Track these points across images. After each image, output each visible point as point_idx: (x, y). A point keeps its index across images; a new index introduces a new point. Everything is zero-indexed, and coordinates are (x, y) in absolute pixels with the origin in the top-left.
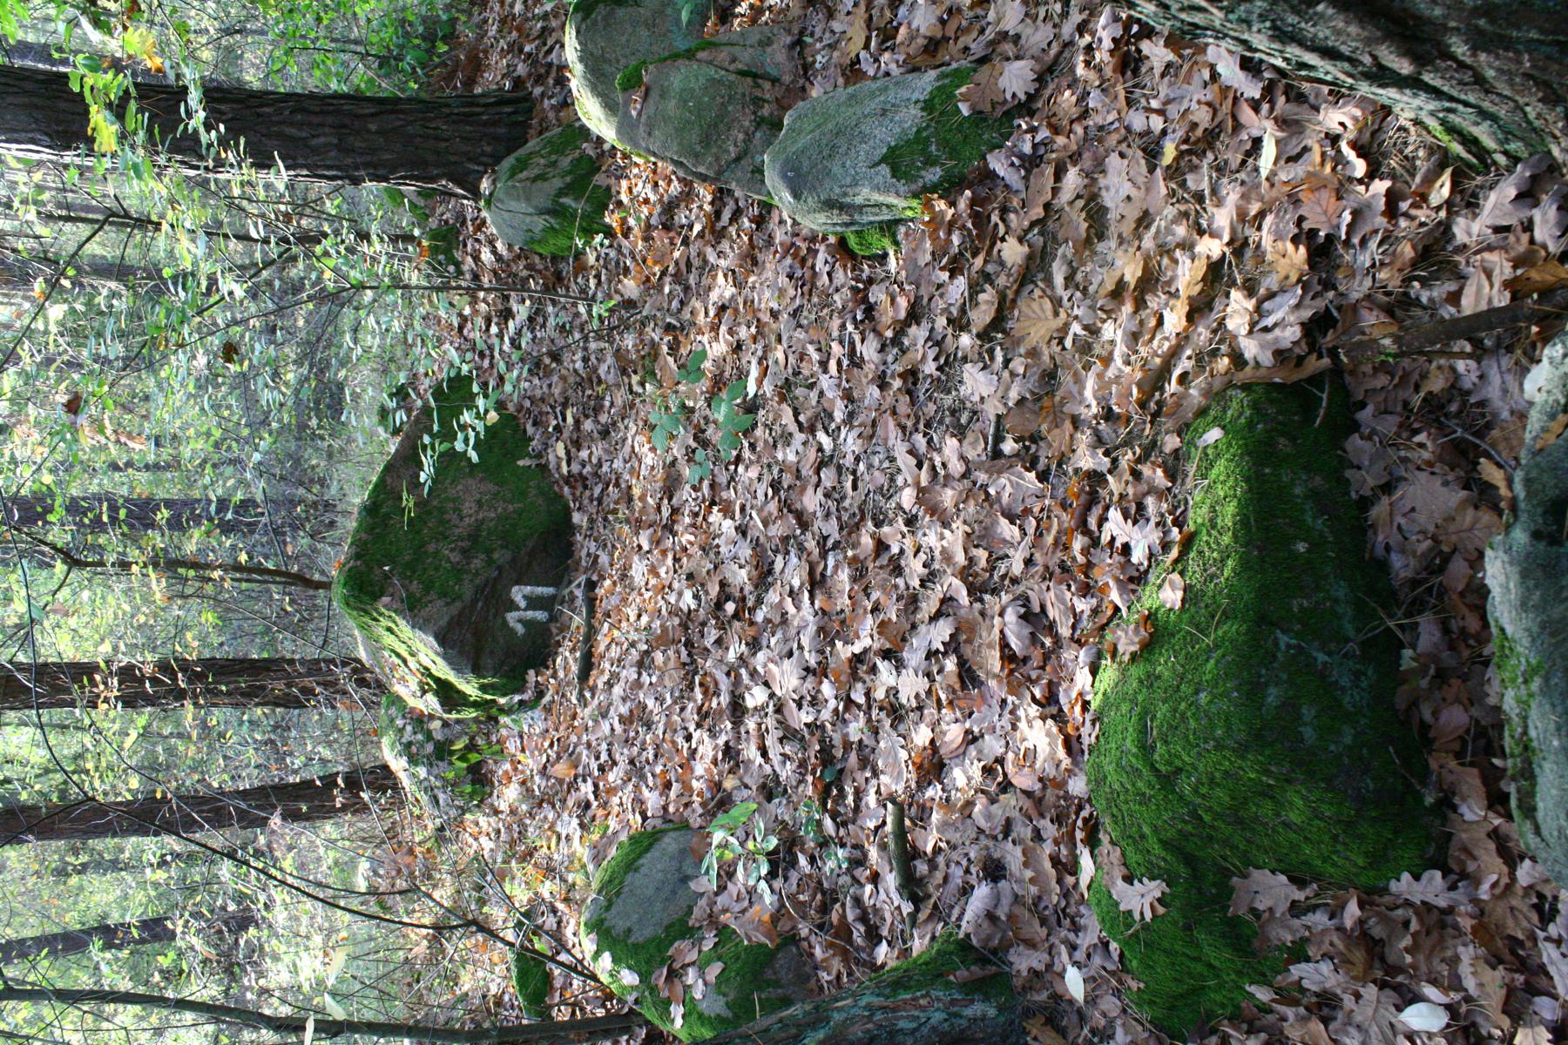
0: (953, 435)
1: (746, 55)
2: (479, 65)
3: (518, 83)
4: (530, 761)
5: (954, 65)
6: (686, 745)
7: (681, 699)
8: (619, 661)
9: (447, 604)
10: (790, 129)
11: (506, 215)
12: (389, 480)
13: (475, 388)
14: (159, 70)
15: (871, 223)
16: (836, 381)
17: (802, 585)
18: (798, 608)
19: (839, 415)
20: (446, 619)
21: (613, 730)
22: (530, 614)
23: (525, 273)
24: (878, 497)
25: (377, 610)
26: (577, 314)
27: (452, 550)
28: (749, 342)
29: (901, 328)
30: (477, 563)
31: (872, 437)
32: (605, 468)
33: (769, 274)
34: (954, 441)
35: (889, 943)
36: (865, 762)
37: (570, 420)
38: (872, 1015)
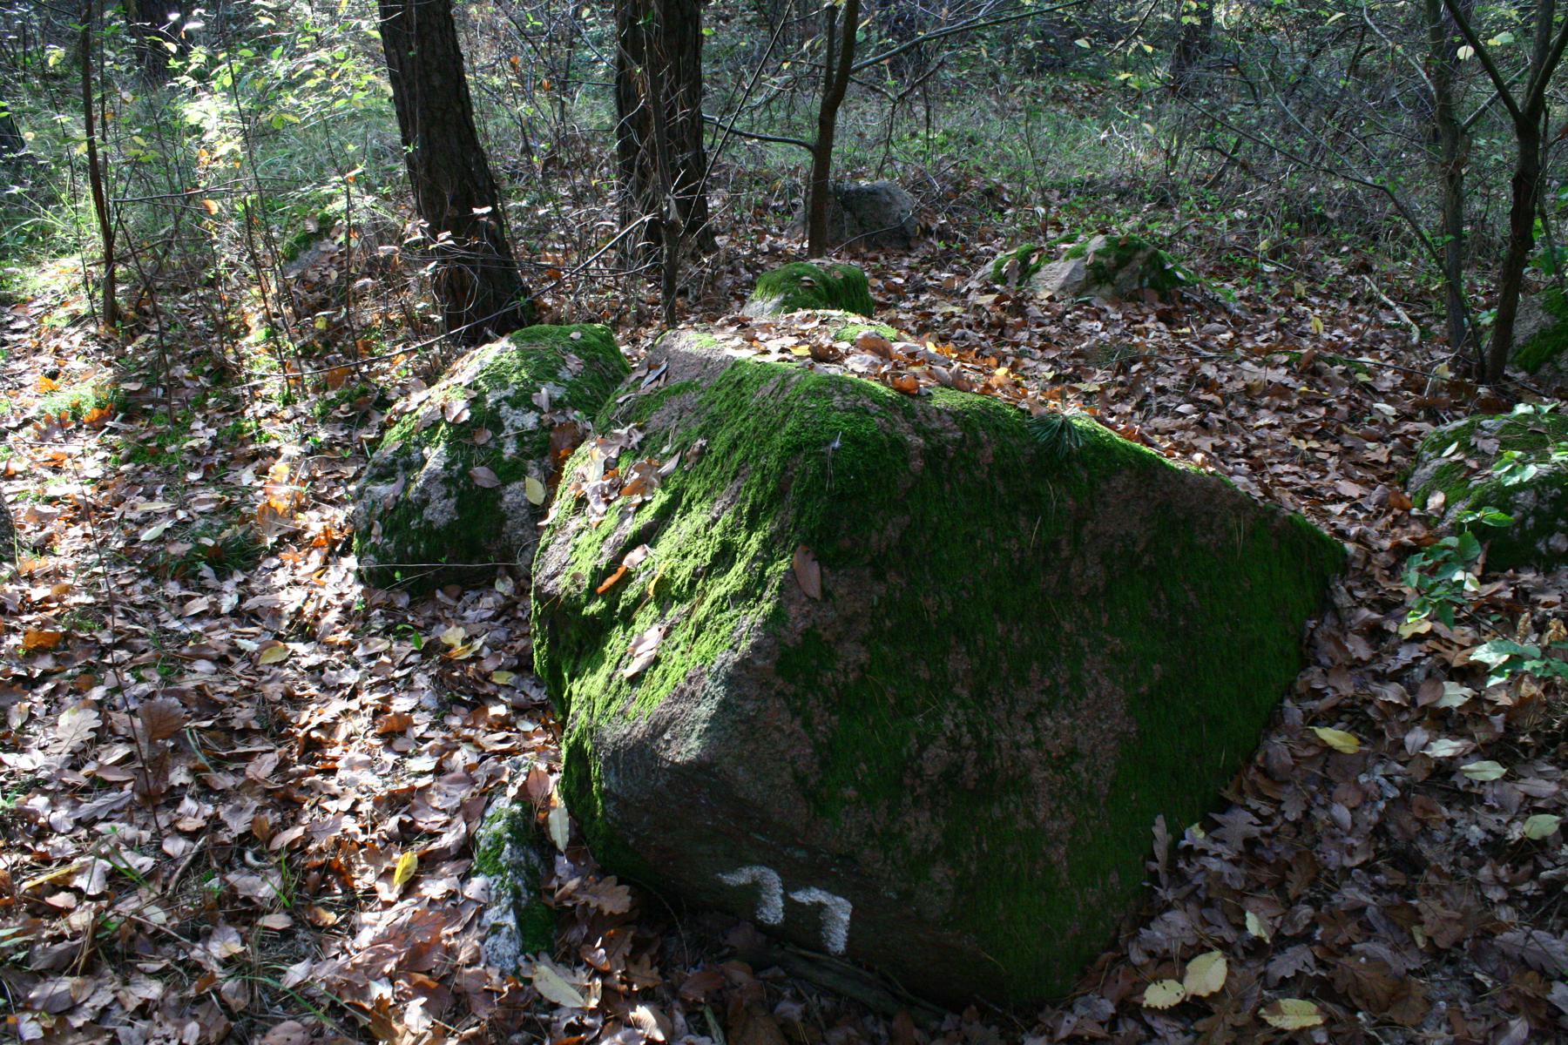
9: (799, 779)
27: (954, 743)
30: (922, 827)
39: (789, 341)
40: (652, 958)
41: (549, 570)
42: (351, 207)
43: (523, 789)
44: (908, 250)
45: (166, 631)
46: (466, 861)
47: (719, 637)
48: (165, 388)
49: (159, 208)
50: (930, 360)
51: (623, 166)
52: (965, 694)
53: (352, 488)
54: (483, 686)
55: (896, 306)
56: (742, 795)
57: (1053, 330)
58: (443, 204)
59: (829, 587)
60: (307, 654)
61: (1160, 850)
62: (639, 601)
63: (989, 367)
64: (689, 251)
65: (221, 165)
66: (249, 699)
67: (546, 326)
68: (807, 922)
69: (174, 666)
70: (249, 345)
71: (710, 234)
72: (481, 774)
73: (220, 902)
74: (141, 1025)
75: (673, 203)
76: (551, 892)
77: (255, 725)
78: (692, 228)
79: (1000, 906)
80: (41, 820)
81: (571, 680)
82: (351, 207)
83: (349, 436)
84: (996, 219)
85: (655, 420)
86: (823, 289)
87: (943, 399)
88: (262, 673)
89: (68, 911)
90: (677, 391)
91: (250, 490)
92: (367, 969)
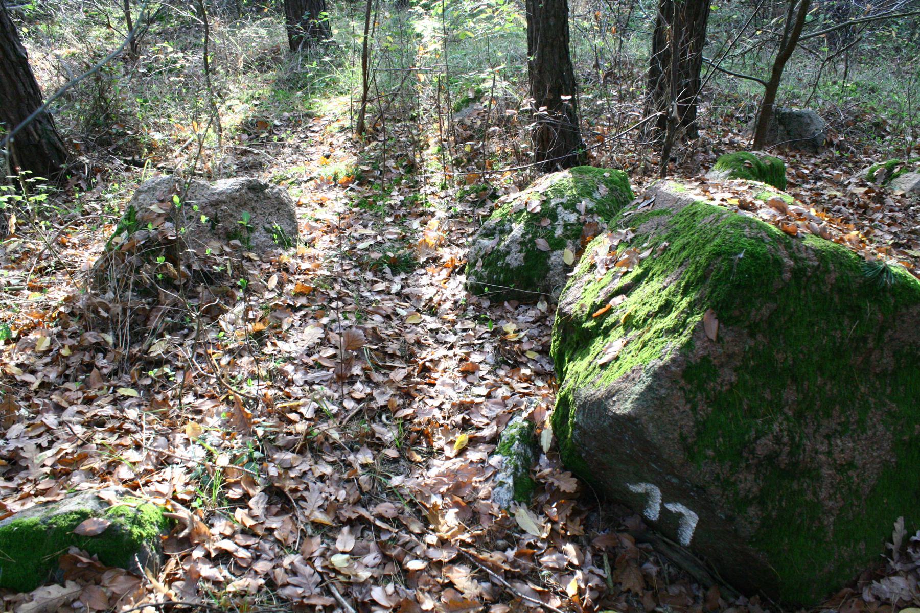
9: (683, 438)
27: (778, 440)
30: (748, 483)
39: (727, 195)
40: (581, 521)
41: (568, 301)
42: (494, 86)
43: (531, 414)
44: (816, 153)
45: (362, 297)
46: (493, 446)
47: (654, 351)
48: (381, 171)
49: (392, 74)
50: (811, 219)
51: (651, 82)
52: (790, 413)
53: (470, 239)
54: (520, 357)
55: (800, 186)
56: (649, 439)
57: (900, 215)
58: (545, 91)
59: (721, 335)
60: (432, 323)
61: (897, 537)
62: (614, 325)
63: (848, 229)
64: (681, 136)
65: (428, 56)
66: (398, 340)
67: (591, 167)
68: (671, 522)
69: (363, 315)
70: (428, 155)
71: (695, 128)
72: (510, 403)
73: (367, 435)
74: (319, 484)
75: (675, 107)
76: (535, 472)
77: (398, 353)
78: (684, 123)
79: (786, 541)
80: (289, 377)
81: (569, 361)
82: (494, 86)
83: (473, 211)
84: (878, 141)
85: (642, 228)
86: (757, 170)
87: (811, 241)
88: (406, 328)
89: (296, 422)
90: (658, 214)
91: (415, 231)
92: (431, 488)
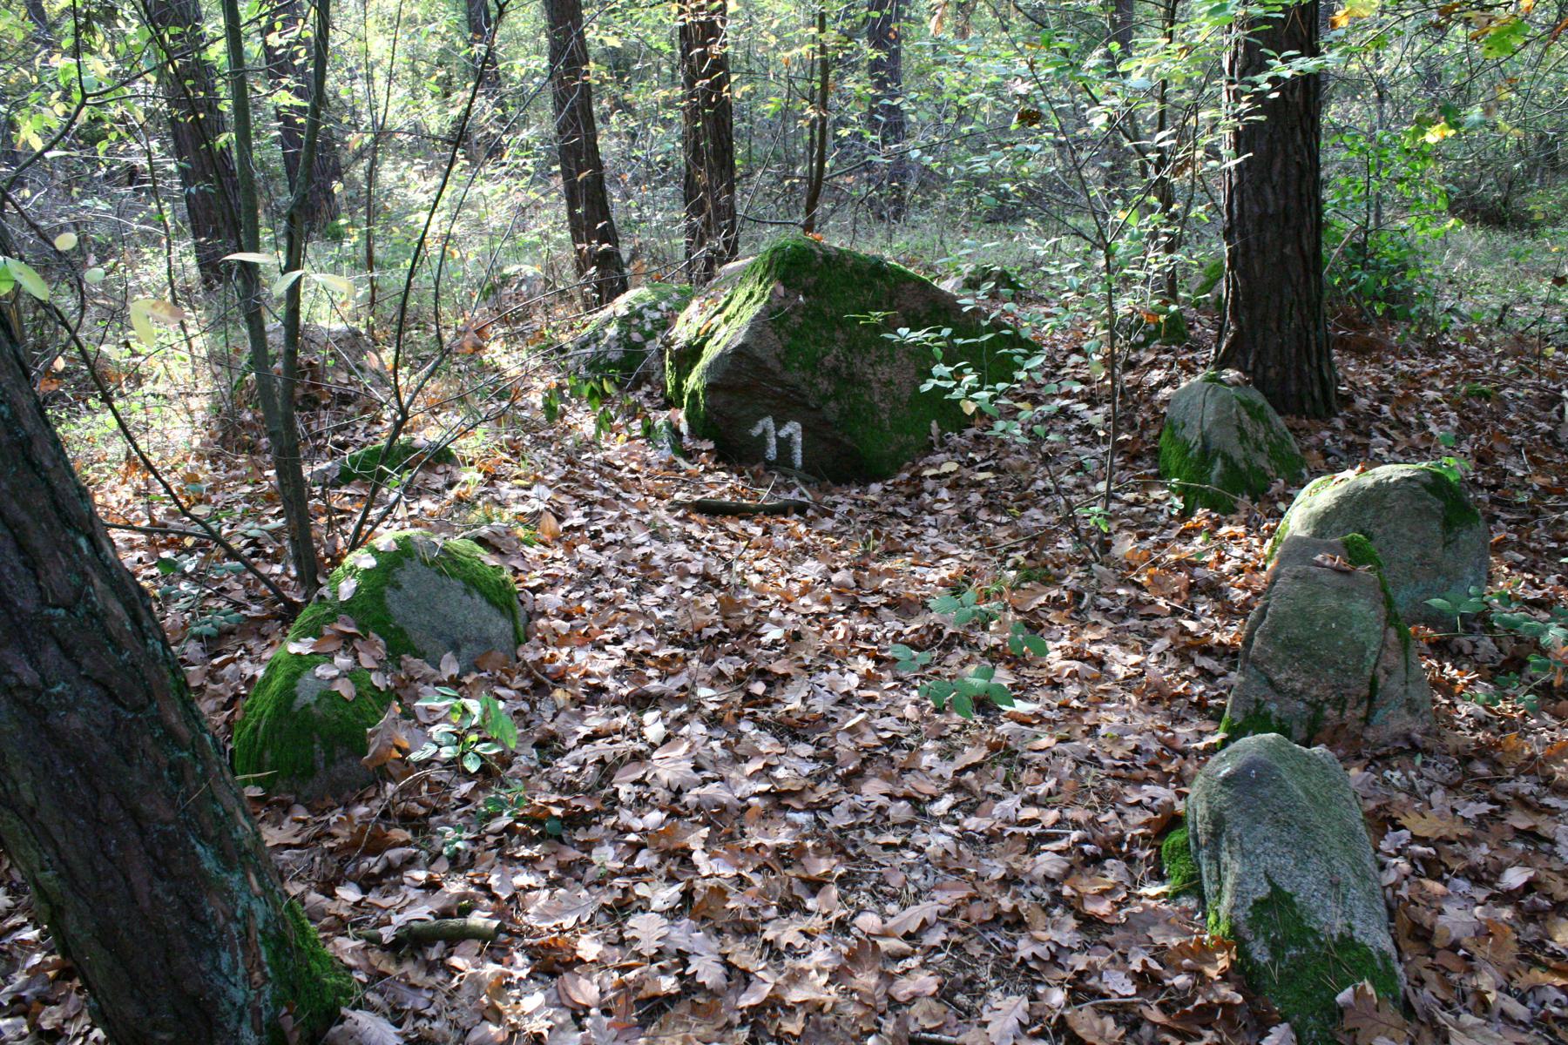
0: (940, 986)
1: (1396, 686)
2: (1363, 353)
3: (1347, 400)
4: (618, 447)
5: (1399, 969)
6: (608, 637)
7: (659, 630)
8: (714, 550)
9: (778, 356)
10: (1309, 759)
11: (1199, 399)
12: (911, 286)
13: (1001, 386)
14: (1334, 24)
15: (1200, 866)
16: (1012, 818)
17: (778, 781)
18: (751, 777)
19: (972, 823)
20: (763, 355)
21: (638, 546)
22: (773, 441)
23: (1139, 420)
24: (874, 878)
25: (769, 282)
26: (1095, 481)
27: (837, 358)
28: (1061, 700)
29: (1073, 906)
30: (824, 385)
31: (944, 868)
32: (929, 519)
33: (1141, 721)
34: (934, 988)
35: (357, 904)
36: (566, 868)
37: (981, 476)
38: (237, 921)
